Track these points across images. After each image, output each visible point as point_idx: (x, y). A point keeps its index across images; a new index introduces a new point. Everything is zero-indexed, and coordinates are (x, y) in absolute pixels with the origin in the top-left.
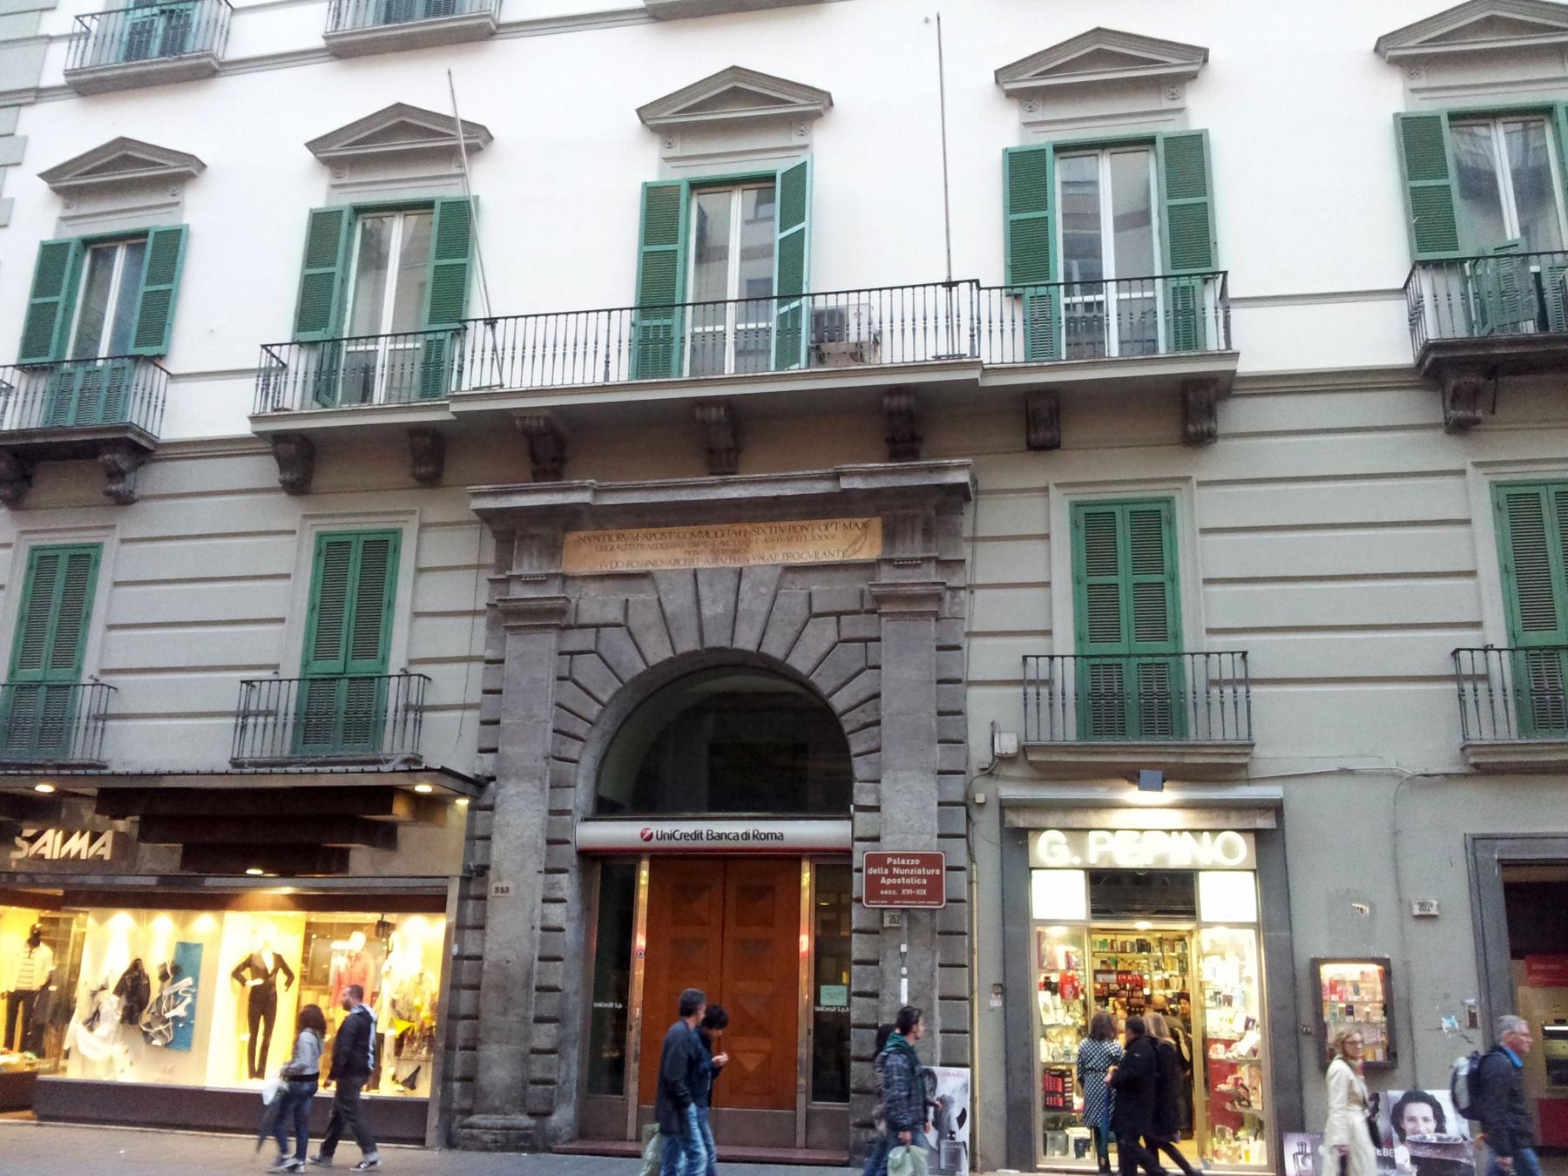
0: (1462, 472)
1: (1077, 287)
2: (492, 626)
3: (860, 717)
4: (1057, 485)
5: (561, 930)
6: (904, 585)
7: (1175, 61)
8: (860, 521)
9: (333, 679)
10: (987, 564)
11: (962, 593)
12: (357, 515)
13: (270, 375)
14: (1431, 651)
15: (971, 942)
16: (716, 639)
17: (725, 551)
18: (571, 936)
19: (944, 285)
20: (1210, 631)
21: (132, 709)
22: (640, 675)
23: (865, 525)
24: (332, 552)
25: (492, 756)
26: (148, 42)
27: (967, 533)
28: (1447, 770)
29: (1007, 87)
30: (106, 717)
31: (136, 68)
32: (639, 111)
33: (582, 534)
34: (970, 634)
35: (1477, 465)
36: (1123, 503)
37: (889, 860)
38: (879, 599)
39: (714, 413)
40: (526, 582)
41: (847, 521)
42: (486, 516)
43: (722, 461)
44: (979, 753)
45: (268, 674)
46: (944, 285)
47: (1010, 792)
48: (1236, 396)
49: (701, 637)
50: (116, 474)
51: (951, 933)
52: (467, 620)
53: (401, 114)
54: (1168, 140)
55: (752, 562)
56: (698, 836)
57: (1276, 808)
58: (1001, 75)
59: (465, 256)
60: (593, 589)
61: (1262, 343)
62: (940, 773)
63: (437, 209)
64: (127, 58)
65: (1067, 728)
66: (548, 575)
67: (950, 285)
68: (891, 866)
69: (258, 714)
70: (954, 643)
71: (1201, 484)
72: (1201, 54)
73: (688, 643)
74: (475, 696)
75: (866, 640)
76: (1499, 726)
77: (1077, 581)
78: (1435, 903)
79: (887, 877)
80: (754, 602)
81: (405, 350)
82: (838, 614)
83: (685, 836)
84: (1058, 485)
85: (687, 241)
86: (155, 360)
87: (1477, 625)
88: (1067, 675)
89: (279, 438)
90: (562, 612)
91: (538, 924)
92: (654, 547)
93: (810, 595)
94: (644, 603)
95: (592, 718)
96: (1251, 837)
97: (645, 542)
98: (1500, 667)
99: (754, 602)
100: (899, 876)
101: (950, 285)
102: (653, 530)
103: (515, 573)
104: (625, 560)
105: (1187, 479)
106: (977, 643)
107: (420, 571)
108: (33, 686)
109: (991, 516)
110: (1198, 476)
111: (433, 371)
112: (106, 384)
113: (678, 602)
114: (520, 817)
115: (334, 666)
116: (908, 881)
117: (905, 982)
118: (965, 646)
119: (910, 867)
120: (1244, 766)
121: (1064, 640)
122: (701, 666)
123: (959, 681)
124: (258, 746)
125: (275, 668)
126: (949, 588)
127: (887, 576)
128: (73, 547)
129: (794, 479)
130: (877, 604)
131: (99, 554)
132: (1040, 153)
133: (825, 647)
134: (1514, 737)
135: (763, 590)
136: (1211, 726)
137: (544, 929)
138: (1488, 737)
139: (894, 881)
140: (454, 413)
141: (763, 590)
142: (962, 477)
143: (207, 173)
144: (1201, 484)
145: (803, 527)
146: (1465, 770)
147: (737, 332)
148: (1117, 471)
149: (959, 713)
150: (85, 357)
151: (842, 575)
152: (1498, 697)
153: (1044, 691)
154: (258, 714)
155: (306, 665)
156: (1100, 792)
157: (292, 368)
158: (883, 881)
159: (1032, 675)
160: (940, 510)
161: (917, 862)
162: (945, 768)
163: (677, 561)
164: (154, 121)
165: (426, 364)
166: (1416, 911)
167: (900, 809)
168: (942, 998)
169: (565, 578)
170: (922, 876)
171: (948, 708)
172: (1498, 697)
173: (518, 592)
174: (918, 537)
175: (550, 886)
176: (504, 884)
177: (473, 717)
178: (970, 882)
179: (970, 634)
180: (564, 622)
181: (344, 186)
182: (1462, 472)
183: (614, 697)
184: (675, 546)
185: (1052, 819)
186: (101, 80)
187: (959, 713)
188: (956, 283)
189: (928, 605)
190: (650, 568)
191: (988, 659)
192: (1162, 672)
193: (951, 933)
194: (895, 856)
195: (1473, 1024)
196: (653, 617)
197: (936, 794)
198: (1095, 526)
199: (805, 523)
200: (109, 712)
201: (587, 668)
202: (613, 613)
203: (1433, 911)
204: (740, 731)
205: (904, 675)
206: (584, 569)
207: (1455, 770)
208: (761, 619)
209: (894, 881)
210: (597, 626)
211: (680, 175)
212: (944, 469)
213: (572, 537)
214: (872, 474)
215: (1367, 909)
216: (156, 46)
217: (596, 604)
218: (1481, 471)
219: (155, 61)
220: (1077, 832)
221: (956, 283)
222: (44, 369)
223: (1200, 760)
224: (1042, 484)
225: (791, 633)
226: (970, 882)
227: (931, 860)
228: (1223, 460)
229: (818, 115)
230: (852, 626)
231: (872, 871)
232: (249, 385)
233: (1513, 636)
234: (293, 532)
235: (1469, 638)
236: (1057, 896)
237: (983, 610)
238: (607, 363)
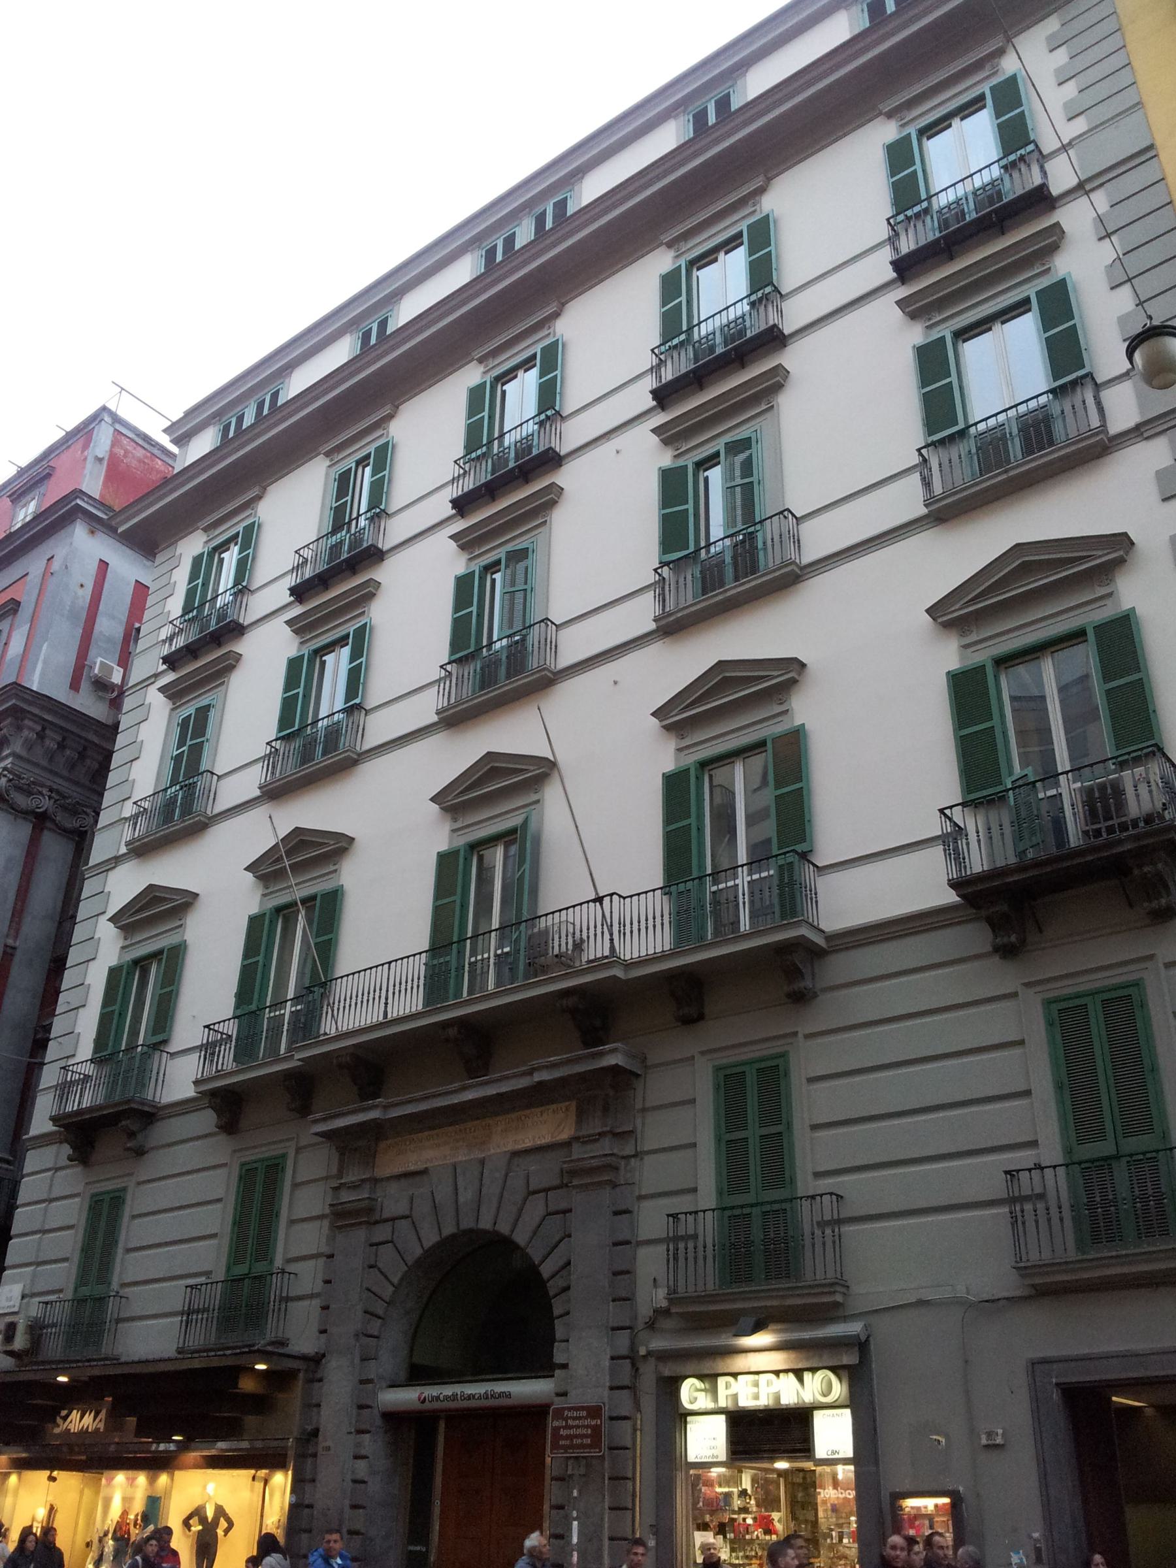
0: (1014, 995)
1: (1038, 785)
3: (559, 1282)
4: (703, 1053)
5: (364, 1482)
7: (1100, 553)
9: (1108, 1160)
10: (656, 1132)
12: (261, 1144)
13: (951, 840)
14: (984, 1177)
16: (467, 1223)
18: (375, 1487)
19: (594, 901)
20: (818, 1175)
21: (138, 1312)
24: (1067, 1019)
26: (496, 672)
27: (639, 1106)
28: (1006, 1294)
29: (940, 620)
30: (288, 1299)
31: (309, 768)
32: (927, 611)
33: (389, 1142)
34: (641, 1198)
35: (1027, 985)
36: (1093, 993)
37: (584, 1413)
38: (573, 1173)
39: (452, 1032)
41: (554, 1106)
42: (328, 1135)
44: (644, 1312)
45: (203, 1279)
46: (594, 901)
47: (658, 1343)
48: (163, 1119)
50: (132, 1135)
52: (317, 1223)
53: (723, 671)
54: (1100, 629)
55: (492, 1151)
56: (454, 1397)
57: (862, 1345)
58: (933, 611)
59: (331, 932)
60: (393, 1188)
61: (846, 901)
62: (613, 1329)
63: (769, 745)
64: (482, 688)
65: (708, 1278)
67: (599, 900)
68: (566, 1419)
69: (198, 1311)
70: (624, 1208)
71: (808, 1036)
72: (798, 665)
76: (1057, 1243)
77: (718, 1140)
78: (1000, 1431)
79: (565, 1428)
81: (727, 887)
83: (447, 1398)
84: (703, 1053)
85: (1002, 716)
86: (805, 856)
87: (1034, 1144)
88: (708, 1228)
89: (213, 1093)
90: (370, 1210)
91: (349, 1477)
96: (845, 1375)
98: (1058, 1184)
104: (412, 1161)
105: (795, 1034)
106: (646, 1204)
107: (296, 1186)
108: (239, 1280)
109: (659, 1087)
110: (804, 1029)
111: (305, 1025)
112: (137, 1065)
113: (443, 1193)
114: (338, 1386)
115: (1106, 1148)
116: (579, 1431)
117: (575, 1523)
119: (579, 1418)
120: (837, 1305)
121: (707, 1197)
123: (628, 1243)
124: (198, 1338)
125: (207, 1274)
126: (623, 1157)
127: (577, 1152)
128: (762, 1060)
129: (507, 1078)
130: (571, 1176)
131: (787, 1062)
132: (981, 668)
133: (537, 1220)
134: (1072, 1255)
135: (497, 1175)
136: (816, 1267)
138: (1047, 1255)
141: (497, 1175)
143: (356, 843)
144: (808, 1036)
146: (1026, 1293)
147: (496, 955)
148: (736, 1034)
149: (628, 1272)
150: (131, 1048)
152: (1054, 1211)
153: (691, 1245)
154: (198, 1311)
155: (228, 1269)
156: (724, 1340)
157: (971, 829)
159: (681, 1232)
161: (584, 1413)
162: (616, 1325)
163: (445, 1157)
164: (316, 812)
165: (781, 886)
166: (984, 1441)
167: (585, 1364)
168: (611, 1539)
169: (375, 1181)
170: (587, 1427)
171: (620, 1268)
172: (1054, 1211)
173: (346, 1196)
175: (358, 1445)
177: (316, 1303)
178: (635, 1430)
179: (641, 1198)
180: (373, 1220)
181: (271, 893)
182: (1014, 995)
183: (402, 1279)
185: (691, 1367)
186: (145, 844)
187: (628, 1272)
189: (605, 1175)
191: (651, 1220)
192: (781, 1213)
195: (1039, 1560)
197: (608, 1350)
198: (730, 1084)
199: (528, 1112)
200: (291, 1295)
201: (387, 1255)
202: (401, 1208)
203: (999, 1440)
204: (489, 1300)
205: (588, 1244)
207: (1018, 1293)
210: (393, 1219)
211: (982, 656)
212: (601, 1054)
213: (382, 1145)
214: (554, 1066)
215: (943, 1440)
216: (319, 749)
217: (393, 1200)
218: (1031, 991)
219: (320, 760)
220: (710, 1378)
222: (106, 1060)
223: (799, 1301)
227: (594, 1412)
228: (827, 1011)
229: (794, 682)
232: (938, 851)
233: (1068, 1151)
234: (225, 1165)
235: (1023, 1158)
236: (706, 1440)
237: (652, 1174)
238: (386, 1004)
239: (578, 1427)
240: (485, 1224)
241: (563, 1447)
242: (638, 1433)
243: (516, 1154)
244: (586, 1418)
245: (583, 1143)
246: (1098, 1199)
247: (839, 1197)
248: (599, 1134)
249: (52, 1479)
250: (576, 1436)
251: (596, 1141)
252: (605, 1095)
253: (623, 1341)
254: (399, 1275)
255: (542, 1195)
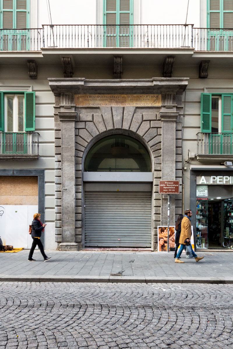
2: (56, 120)
6: (168, 113)
8: (156, 95)
11: (182, 116)
15: (182, 201)
16: (118, 126)
17: (119, 102)
22: (98, 135)
23: (157, 96)
25: (59, 155)
27: (183, 100)
33: (80, 95)
37: (173, 183)
40: (65, 108)
41: (152, 95)
43: (117, 75)
44: (186, 158)
49: (122, 126)
51: (178, 200)
60: (84, 111)
66: (71, 106)
67: (186, 25)
73: (110, 127)
74: (54, 140)
75: (157, 128)
79: (165, 187)
80: (128, 116)
82: (150, 121)
84: (207, 88)
92: (100, 100)
93: (143, 115)
94: (98, 116)
95: (85, 146)
97: (97, 98)
99: (128, 116)
100: (168, 186)
101: (186, 25)
102: (100, 95)
103: (62, 105)
116: (170, 188)
117: (169, 211)
118: (182, 130)
122: (111, 134)
127: (163, 110)
135: (130, 113)
137: (76, 199)
139: (167, 188)
140: (43, 55)
141: (130, 113)
142: (186, 83)
145: (140, 96)
151: (151, 110)
158: (164, 187)
160: (177, 93)
161: (173, 183)
169: (76, 108)
170: (174, 187)
173: (62, 110)
174: (172, 100)
176: (66, 188)
184: (106, 100)
187: (181, 147)
188: (187, 25)
190: (99, 106)
193: (178, 200)
194: (167, 182)
196: (101, 120)
199: (141, 95)
201: (83, 133)
202: (90, 119)
206: (81, 106)
208: (130, 121)
209: (167, 188)
210: (85, 122)
212: (182, 80)
217: (85, 115)
221: (187, 25)
224: (202, 88)
225: (138, 125)
226: (182, 188)
230: (153, 124)
231: (161, 185)
239: (170, 186)
240: (126, 127)
241: (164, 191)
242: (183, 189)
243: (137, 108)
244: (173, 184)
245: (167, 108)
246: (217, 142)
247: (39, 134)
248: (173, 106)
249: (74, 199)
250: (170, 189)
251: (172, 108)
252: (175, 94)
253: (180, 166)
254: (90, 139)
255: (149, 122)
